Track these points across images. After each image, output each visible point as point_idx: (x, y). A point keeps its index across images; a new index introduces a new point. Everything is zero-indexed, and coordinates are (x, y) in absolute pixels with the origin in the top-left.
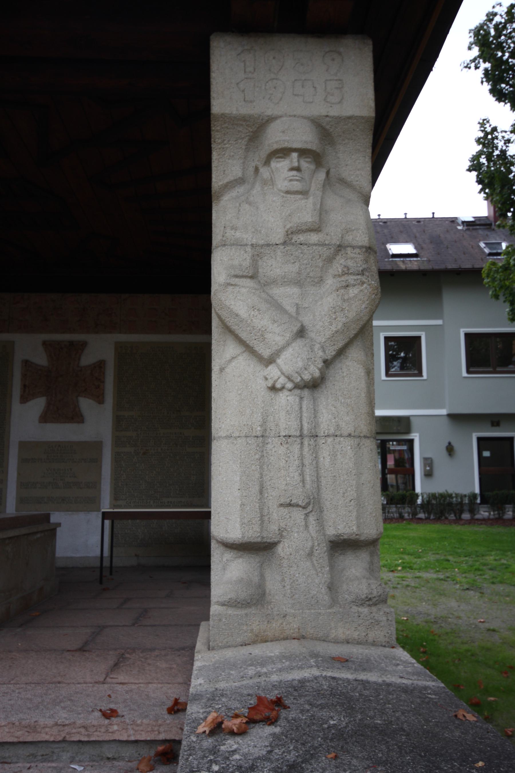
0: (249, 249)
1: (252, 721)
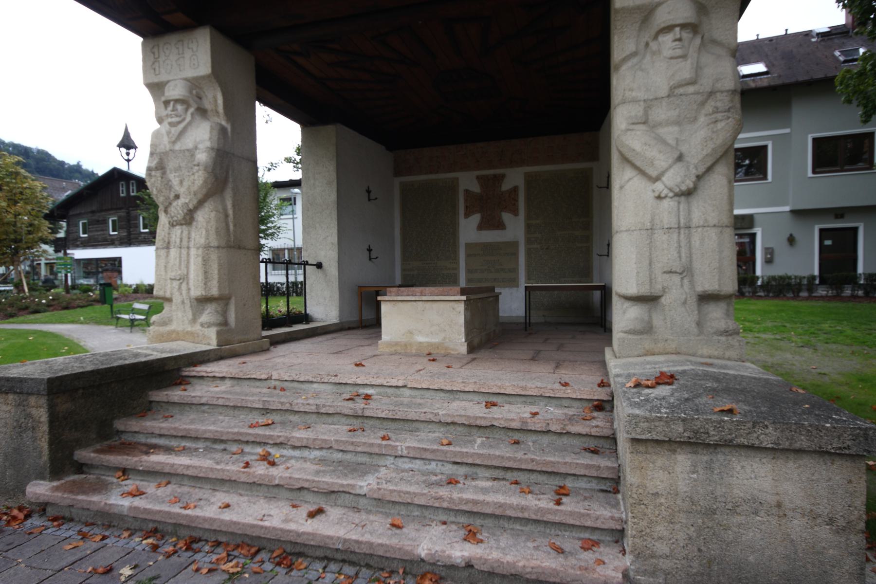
0: (642, 103)
1: (658, 384)
